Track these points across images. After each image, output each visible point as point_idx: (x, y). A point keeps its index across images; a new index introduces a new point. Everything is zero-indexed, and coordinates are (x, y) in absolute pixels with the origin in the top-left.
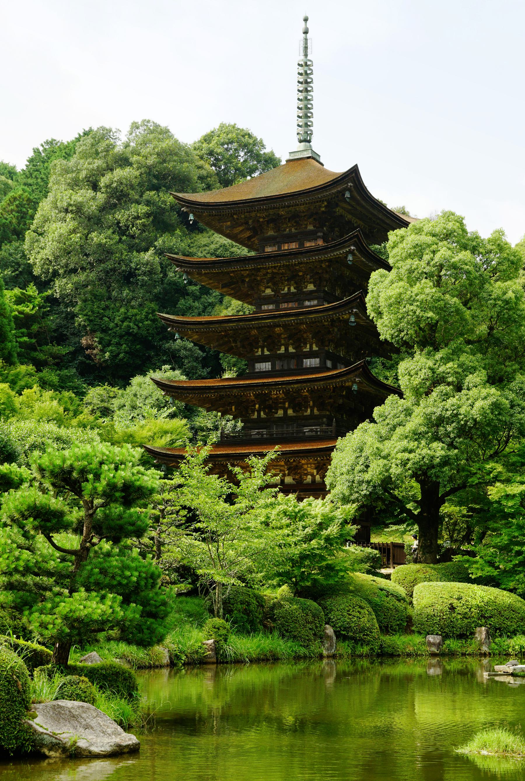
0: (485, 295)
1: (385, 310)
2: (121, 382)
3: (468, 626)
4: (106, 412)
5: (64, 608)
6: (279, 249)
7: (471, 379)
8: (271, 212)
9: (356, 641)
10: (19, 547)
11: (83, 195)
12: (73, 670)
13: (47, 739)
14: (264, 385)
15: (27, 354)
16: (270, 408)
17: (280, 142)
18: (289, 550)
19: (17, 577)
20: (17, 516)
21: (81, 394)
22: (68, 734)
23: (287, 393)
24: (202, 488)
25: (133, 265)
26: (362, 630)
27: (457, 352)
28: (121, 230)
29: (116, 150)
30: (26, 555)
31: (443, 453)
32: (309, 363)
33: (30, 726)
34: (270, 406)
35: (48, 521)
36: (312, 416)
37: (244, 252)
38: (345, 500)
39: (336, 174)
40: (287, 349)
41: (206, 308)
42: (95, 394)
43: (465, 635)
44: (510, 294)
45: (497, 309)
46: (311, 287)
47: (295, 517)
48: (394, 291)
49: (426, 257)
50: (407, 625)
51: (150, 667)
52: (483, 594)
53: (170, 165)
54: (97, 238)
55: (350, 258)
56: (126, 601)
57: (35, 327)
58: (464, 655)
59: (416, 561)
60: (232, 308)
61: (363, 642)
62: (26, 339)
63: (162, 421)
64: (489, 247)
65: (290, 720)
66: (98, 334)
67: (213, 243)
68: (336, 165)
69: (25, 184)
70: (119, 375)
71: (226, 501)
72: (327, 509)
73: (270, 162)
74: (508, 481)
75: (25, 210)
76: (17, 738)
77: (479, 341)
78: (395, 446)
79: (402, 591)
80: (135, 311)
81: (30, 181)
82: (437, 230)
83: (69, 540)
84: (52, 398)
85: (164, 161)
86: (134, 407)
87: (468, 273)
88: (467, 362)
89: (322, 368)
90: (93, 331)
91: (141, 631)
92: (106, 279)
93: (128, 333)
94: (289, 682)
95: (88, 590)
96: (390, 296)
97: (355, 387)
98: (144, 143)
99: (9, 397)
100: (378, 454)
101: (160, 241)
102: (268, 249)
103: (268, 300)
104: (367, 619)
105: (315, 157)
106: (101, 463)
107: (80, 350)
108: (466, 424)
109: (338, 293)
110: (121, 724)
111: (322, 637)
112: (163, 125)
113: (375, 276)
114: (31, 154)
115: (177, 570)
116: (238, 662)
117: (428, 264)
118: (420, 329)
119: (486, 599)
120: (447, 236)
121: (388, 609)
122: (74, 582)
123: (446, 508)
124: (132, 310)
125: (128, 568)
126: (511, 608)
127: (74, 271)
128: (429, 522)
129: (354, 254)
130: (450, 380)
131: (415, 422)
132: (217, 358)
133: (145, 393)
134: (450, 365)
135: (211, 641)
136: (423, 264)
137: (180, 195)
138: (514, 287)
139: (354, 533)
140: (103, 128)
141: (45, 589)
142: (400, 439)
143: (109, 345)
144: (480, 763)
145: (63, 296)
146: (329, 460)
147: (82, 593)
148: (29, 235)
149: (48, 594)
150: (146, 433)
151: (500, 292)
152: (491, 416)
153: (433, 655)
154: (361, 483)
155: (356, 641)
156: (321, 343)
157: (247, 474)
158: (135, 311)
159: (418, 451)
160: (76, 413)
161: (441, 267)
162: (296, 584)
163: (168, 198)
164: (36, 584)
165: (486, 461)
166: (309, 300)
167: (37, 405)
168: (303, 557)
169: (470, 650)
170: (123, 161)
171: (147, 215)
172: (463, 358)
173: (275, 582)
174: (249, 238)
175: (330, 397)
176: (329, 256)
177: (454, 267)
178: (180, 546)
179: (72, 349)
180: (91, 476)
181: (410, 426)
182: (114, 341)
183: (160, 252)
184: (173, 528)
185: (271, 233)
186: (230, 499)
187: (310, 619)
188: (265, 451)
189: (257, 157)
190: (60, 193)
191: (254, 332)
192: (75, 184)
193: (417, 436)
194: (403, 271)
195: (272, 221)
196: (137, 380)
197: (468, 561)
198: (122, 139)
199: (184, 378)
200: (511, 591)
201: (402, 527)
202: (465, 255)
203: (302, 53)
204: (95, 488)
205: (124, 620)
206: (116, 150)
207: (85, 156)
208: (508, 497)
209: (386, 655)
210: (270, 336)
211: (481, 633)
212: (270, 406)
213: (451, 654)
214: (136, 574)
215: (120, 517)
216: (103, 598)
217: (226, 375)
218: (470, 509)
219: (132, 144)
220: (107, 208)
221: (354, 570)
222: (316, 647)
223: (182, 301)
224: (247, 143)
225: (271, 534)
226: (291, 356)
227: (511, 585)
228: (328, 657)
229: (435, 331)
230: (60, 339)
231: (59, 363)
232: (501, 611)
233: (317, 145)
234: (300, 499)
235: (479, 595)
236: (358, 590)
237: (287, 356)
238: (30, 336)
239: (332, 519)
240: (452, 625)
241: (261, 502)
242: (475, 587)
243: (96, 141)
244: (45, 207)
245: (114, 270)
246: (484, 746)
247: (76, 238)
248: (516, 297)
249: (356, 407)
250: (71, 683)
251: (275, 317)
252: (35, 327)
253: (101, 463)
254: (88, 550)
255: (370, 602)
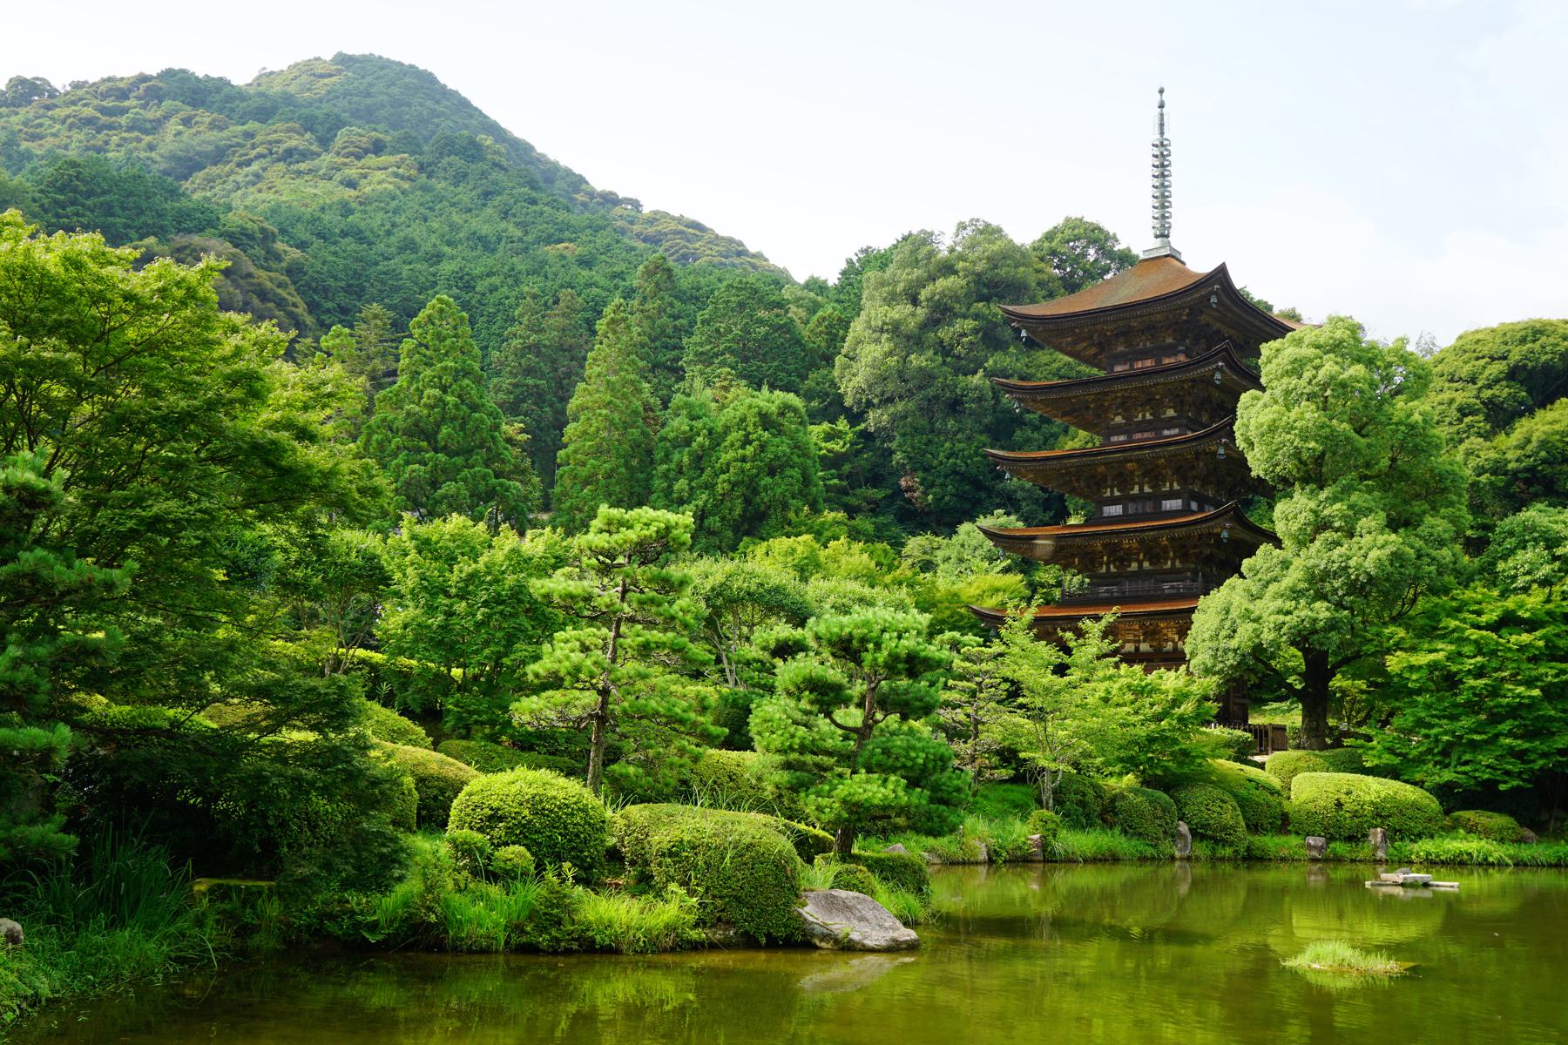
0: (1383, 419)
1: (1256, 441)
2: (946, 530)
3: (1359, 826)
4: (928, 566)
5: (842, 791)
6: (1132, 368)
7: (1364, 523)
8: (1121, 323)
9: (1216, 841)
10: (795, 723)
11: (900, 311)
12: (857, 859)
13: (818, 930)
14: (1112, 533)
15: (837, 498)
16: (1121, 560)
17: (1137, 238)
18: (1132, 730)
19: (794, 756)
20: (792, 689)
21: (898, 544)
22: (841, 926)
23: (1142, 542)
24: (1026, 657)
25: (958, 391)
26: (1224, 828)
27: (1347, 490)
28: (944, 350)
29: (940, 255)
30: (802, 731)
31: (1328, 614)
32: (1169, 505)
33: (800, 915)
34: (1122, 558)
35: (826, 696)
36: (1173, 570)
37: (1087, 370)
38: (1208, 671)
39: (1197, 275)
40: (1141, 489)
41: (1049, 441)
42: (915, 545)
43: (1355, 837)
44: (1417, 417)
45: (1400, 436)
46: (1171, 413)
47: (1139, 692)
48: (1266, 417)
49: (1307, 375)
50: (1284, 823)
51: (964, 863)
52: (1379, 788)
53: (1003, 272)
54: (917, 360)
55: (1218, 376)
56: (913, 783)
57: (847, 468)
58: (1353, 861)
59: (1298, 747)
60: (1078, 440)
61: (1225, 843)
62: (835, 481)
63: (995, 579)
64: (1389, 359)
65: (1136, 931)
66: (920, 474)
67: (1053, 363)
68: (1200, 264)
69: (838, 301)
70: (944, 521)
71: (1054, 672)
72: (1181, 683)
73: (1125, 259)
74: (1413, 649)
75: (836, 332)
76: (786, 926)
77: (1378, 476)
78: (1267, 606)
79: (1276, 782)
80: (962, 445)
81: (842, 297)
82: (1322, 341)
83: (852, 716)
84: (862, 551)
85: (996, 267)
86: (961, 560)
87: (1362, 392)
88: (1360, 503)
89: (1186, 511)
90: (914, 470)
91: (930, 819)
92: (926, 410)
93: (955, 472)
94: (1130, 888)
95: (869, 771)
96: (1263, 424)
97: (1225, 534)
98: (972, 247)
99: (813, 550)
100: (1247, 616)
101: (991, 362)
102: (1118, 368)
103: (1118, 430)
104: (1230, 815)
105: (1174, 255)
106: (883, 631)
107: (899, 492)
108: (1357, 579)
109: (1205, 419)
110: (900, 917)
111: (1175, 836)
112: (994, 223)
113: (1245, 398)
114: (844, 266)
115: (999, 753)
116: (1070, 860)
117: (1309, 383)
118: (1301, 462)
119: (1383, 795)
120: (1335, 347)
121: (1258, 804)
122: (855, 762)
123: (1337, 682)
124: (959, 445)
125: (914, 748)
126: (1415, 806)
127: (890, 400)
128: (1316, 699)
129: (1223, 372)
130: (1337, 524)
131: (1294, 577)
132: (1061, 499)
133: (974, 543)
134: (1338, 506)
135: (1037, 836)
136: (1303, 382)
137: (1010, 308)
138: (1421, 409)
139: (1215, 712)
140: (923, 231)
141: (826, 769)
142: (1274, 598)
143: (932, 486)
144: (1312, 978)
145: (878, 430)
146: (1188, 625)
147: (863, 774)
148: (839, 360)
149: (828, 775)
150: (973, 591)
151: (1402, 415)
152: (1390, 569)
153: (1314, 860)
154: (1226, 651)
155: (1216, 841)
156: (1183, 480)
157: (1081, 641)
158: (962, 445)
159: (1296, 613)
160: (891, 568)
161: (1325, 386)
162: (1143, 772)
163: (996, 310)
164: (817, 765)
165: (1385, 624)
166: (1118, 434)
167: (844, 560)
168: (1151, 740)
169: (1361, 856)
170: (948, 269)
171: (976, 331)
172: (1354, 498)
173: (1117, 769)
174: (1095, 355)
175: (1195, 547)
176: (1190, 375)
177: (1343, 385)
178: (1000, 725)
179: (889, 492)
180: (871, 646)
181: (1287, 582)
182: (938, 481)
183: (989, 374)
184: (993, 704)
185: (1121, 349)
186: (1061, 670)
187: (1159, 813)
188: (1101, 613)
189: (1110, 254)
190: (875, 311)
191: (1102, 469)
192: (891, 299)
193: (1296, 594)
194: (1278, 392)
195: (1124, 334)
196: (965, 527)
197: (1362, 747)
198: (946, 242)
199: (1020, 524)
200: (1415, 783)
201: (1284, 705)
202: (1358, 370)
203: (1157, 131)
204: (875, 659)
205: (908, 806)
206: (940, 255)
207: (903, 265)
208: (1412, 668)
209: (1253, 859)
210: (1120, 474)
211: (1375, 835)
212: (1122, 558)
213: (1338, 860)
214: (923, 755)
215: (907, 692)
216: (885, 781)
217: (1072, 521)
218: (1371, 684)
219: (959, 249)
220: (932, 323)
221: (1214, 757)
222: (1166, 847)
223: (1018, 433)
224: (1097, 237)
225: (1111, 711)
226: (1148, 497)
227: (1418, 777)
228: (1181, 859)
229: (1321, 465)
230: (875, 480)
231: (875, 509)
232: (1402, 809)
233: (1177, 241)
234: (1147, 671)
235: (1374, 789)
236: (1222, 782)
237: (1142, 497)
238: (840, 477)
239: (1186, 696)
240: (1338, 825)
241: (1100, 674)
242: (1370, 779)
243: (916, 246)
244: (858, 327)
245: (936, 397)
246: (1317, 958)
247: (892, 361)
248: (1425, 421)
249: (1221, 562)
250: (848, 872)
251: (1132, 449)
252: (847, 468)
253: (883, 631)
254: (871, 727)
255: (1235, 796)
